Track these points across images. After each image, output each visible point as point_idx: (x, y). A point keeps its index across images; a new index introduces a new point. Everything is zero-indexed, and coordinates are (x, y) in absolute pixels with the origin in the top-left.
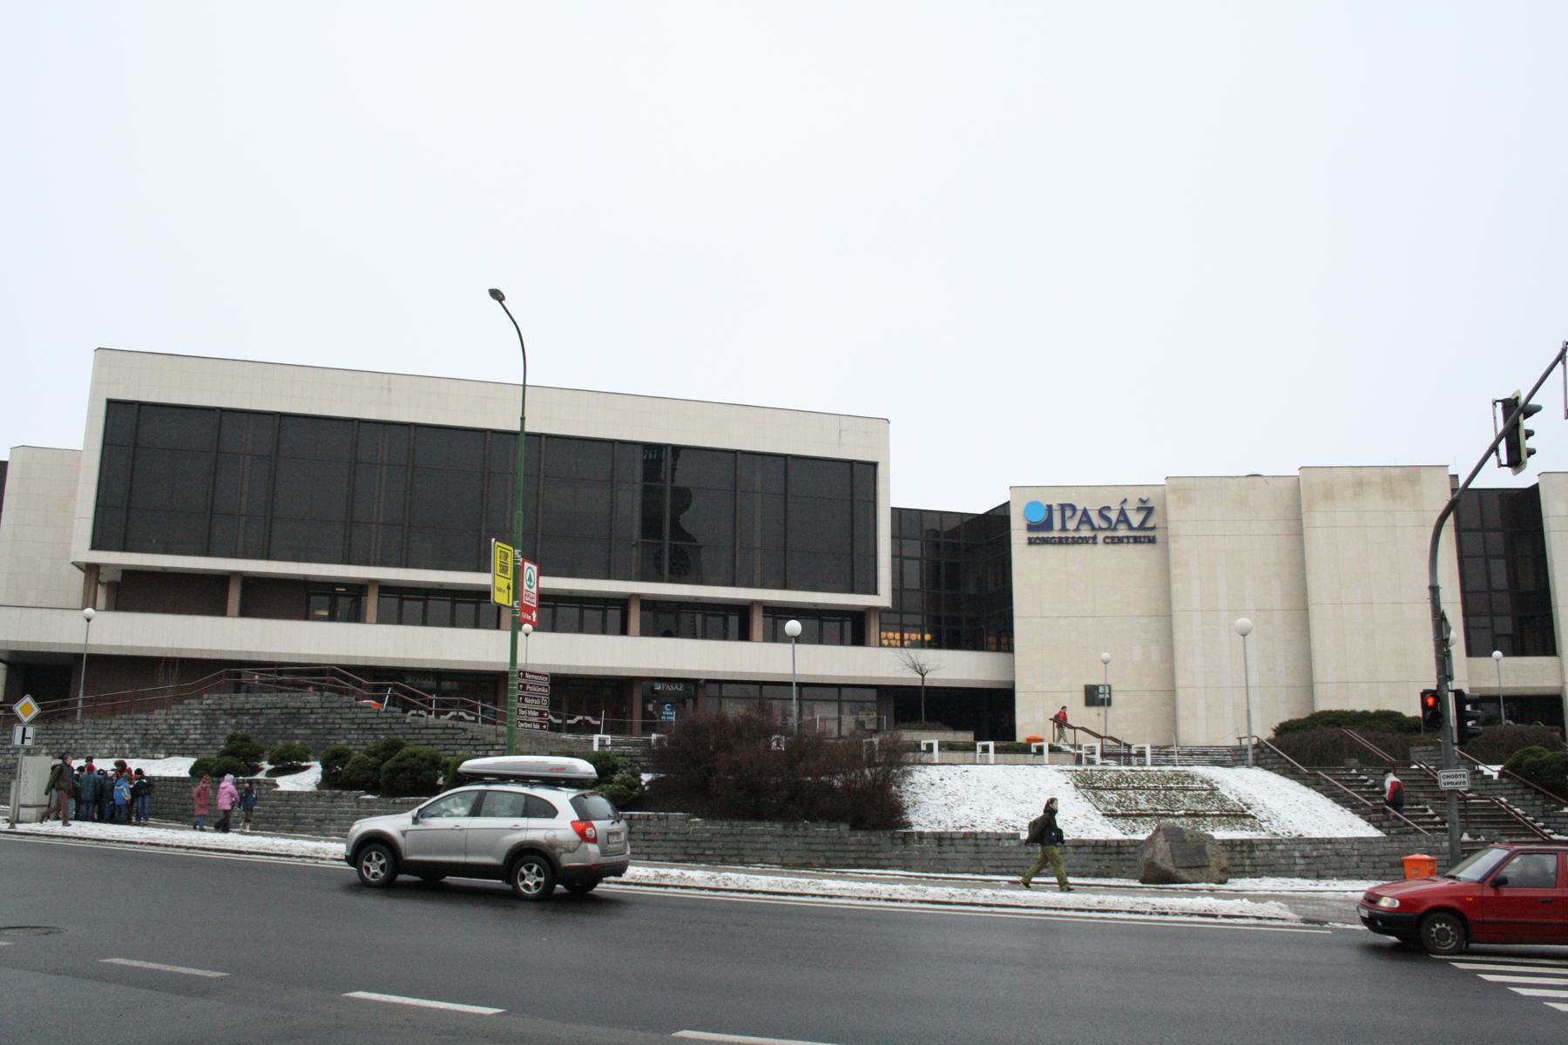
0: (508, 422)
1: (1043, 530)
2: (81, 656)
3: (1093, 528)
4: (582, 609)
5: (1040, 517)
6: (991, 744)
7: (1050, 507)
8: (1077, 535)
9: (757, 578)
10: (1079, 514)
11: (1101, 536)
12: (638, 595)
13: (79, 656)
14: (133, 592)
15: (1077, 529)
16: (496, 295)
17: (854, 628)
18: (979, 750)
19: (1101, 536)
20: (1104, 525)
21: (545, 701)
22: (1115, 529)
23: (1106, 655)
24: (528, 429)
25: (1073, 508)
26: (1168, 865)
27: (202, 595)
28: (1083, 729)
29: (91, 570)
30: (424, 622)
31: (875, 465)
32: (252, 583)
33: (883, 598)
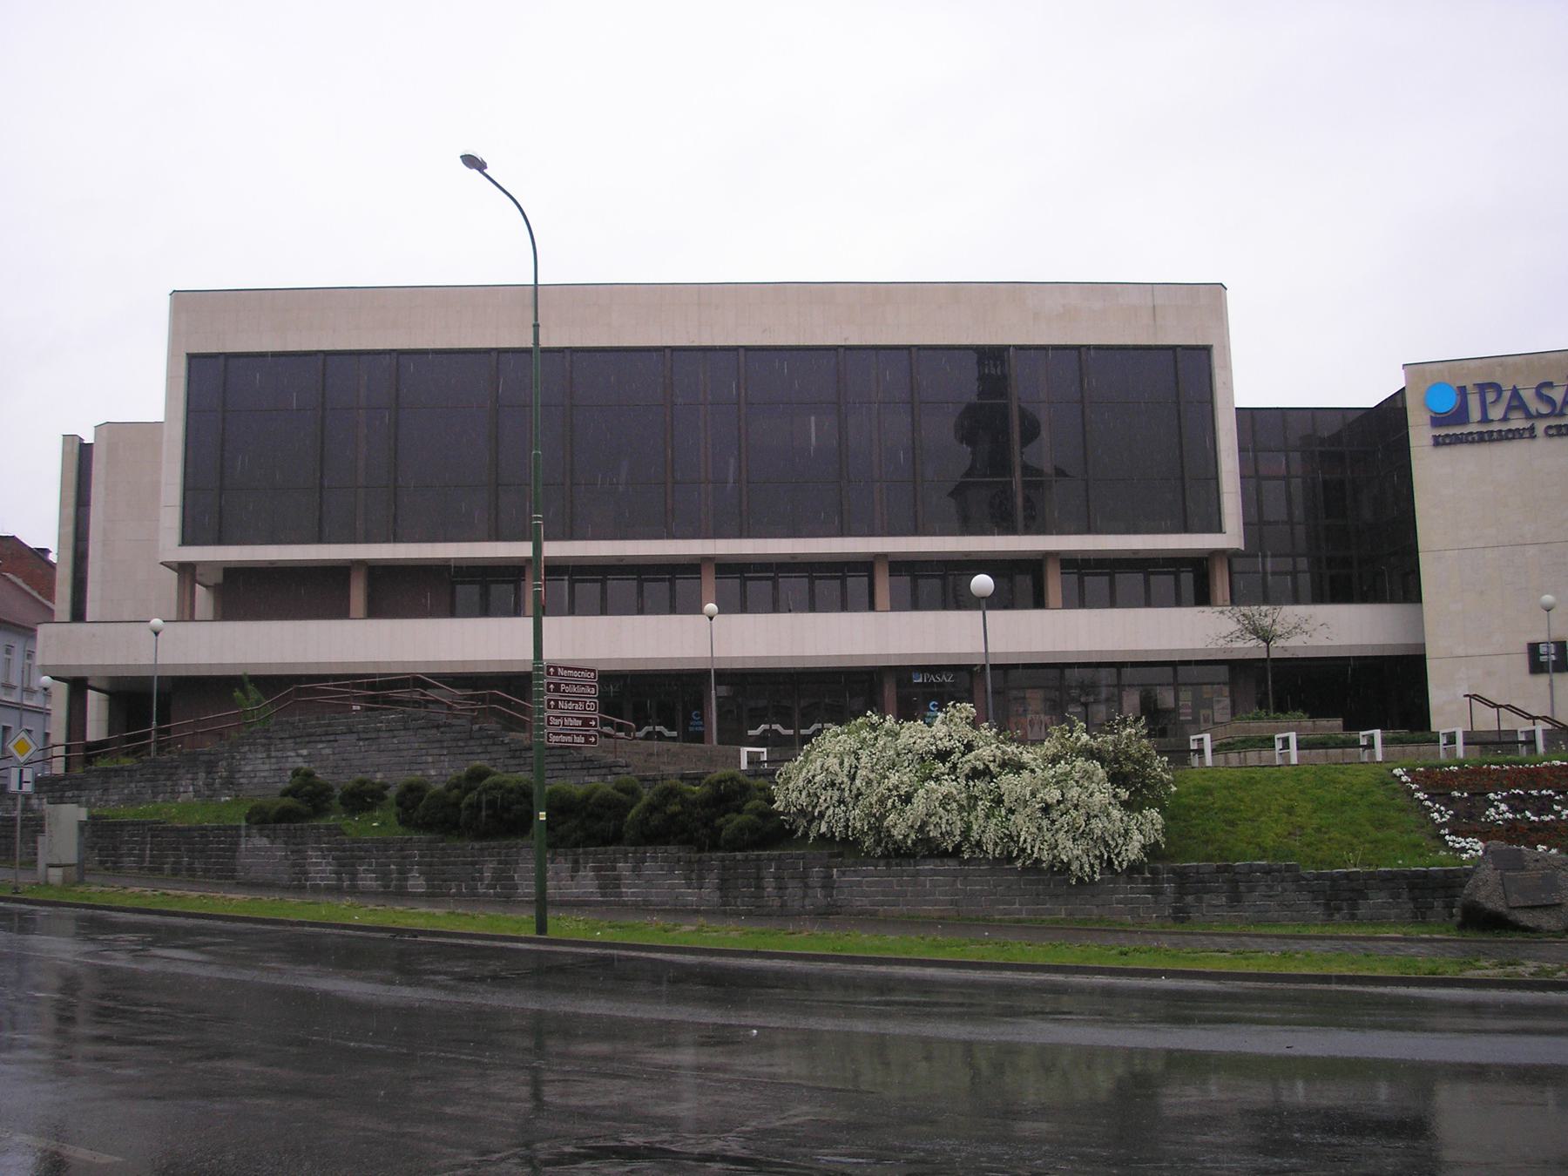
0: (520, 338)
1: (1453, 426)
2: (707, 672)
3: (1529, 416)
4: (744, 580)
5: (1447, 404)
6: (1377, 733)
7: (1462, 391)
8: (1504, 427)
9: (1020, 525)
10: (1507, 395)
11: (1541, 426)
12: (885, 555)
13: (705, 673)
14: (246, 594)
15: (1505, 419)
16: (472, 161)
17: (1192, 581)
18: (1279, 745)
19: (1541, 426)
20: (1545, 410)
21: (592, 703)
22: (1562, 415)
23: (1548, 598)
24: (543, 343)
25: (1497, 388)
26: (1495, 904)
27: (317, 592)
28: (1508, 707)
29: (186, 570)
30: (775, 608)
31: (1207, 349)
32: (379, 573)
33: (1231, 536)
